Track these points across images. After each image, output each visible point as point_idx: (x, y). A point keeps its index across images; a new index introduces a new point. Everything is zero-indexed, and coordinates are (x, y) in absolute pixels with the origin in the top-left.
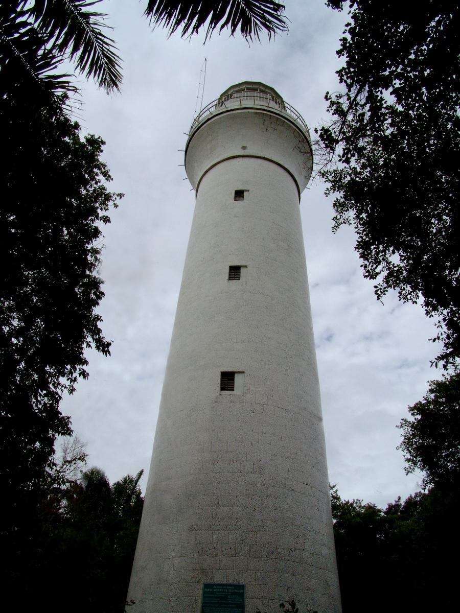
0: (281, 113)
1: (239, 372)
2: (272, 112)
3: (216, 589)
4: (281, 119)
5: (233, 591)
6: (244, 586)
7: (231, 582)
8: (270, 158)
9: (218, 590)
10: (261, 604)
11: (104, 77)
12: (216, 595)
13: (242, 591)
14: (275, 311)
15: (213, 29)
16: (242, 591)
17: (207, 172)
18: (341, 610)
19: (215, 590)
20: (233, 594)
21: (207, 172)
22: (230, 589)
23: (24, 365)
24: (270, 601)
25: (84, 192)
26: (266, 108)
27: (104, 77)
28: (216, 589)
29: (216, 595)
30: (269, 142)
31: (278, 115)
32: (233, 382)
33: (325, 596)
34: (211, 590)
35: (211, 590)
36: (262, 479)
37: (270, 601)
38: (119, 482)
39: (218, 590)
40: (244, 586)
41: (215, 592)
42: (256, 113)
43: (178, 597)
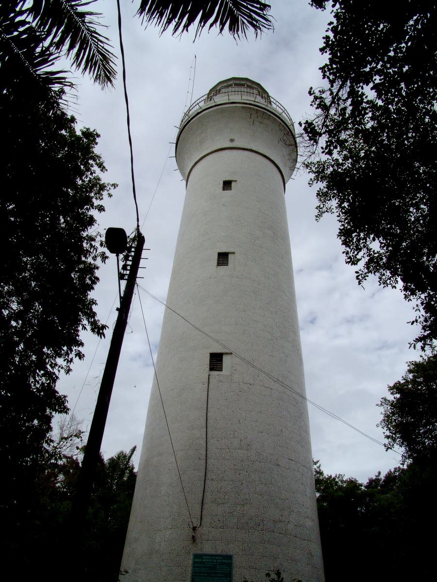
1: (227, 354)
2: (259, 107)
4: (267, 113)
6: (231, 556)
7: (219, 552)
8: (257, 150)
16: (230, 561)
17: (196, 163)
19: (204, 560)
20: (222, 563)
21: (196, 163)
24: (257, 571)
26: (252, 103)
29: (205, 565)
31: (264, 109)
32: (221, 362)
34: (201, 560)
35: (201, 560)
37: (257, 571)
39: (207, 560)
40: (231, 556)
42: (243, 107)
43: (169, 566)
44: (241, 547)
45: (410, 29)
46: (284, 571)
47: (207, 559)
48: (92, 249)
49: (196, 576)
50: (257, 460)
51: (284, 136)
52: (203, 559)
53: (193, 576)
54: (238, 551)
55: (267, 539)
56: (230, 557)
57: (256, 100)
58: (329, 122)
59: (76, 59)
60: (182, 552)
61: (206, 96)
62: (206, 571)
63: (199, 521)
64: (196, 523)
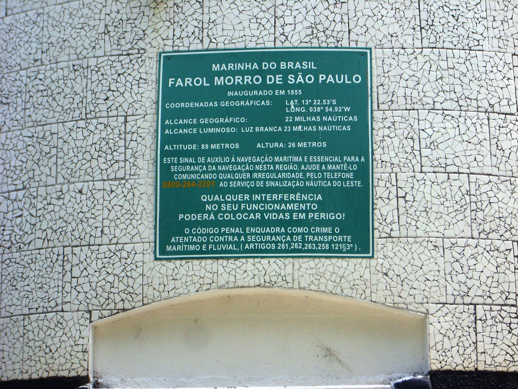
3: (224, 74)
5: (310, 79)
6: (364, 54)
9: (238, 79)
10: (452, 133)
12: (225, 104)
15: (394, 307)
16: (357, 79)
18: (4, 379)
19: (218, 81)
22: (295, 72)
24: (496, 120)
25: (300, 91)
28: (224, 74)
29: (225, 104)
34: (202, 82)
35: (202, 82)
37: (496, 120)
39: (238, 79)
40: (364, 54)
41: (225, 88)
43: (37, 123)
44: (409, 14)
46: (150, 229)
47: (233, 73)
48: (288, 205)
50: (324, 32)
52: (211, 76)
53: (164, 154)
54: (395, 28)
58: (295, 106)
60: (99, 52)
62: (233, 130)
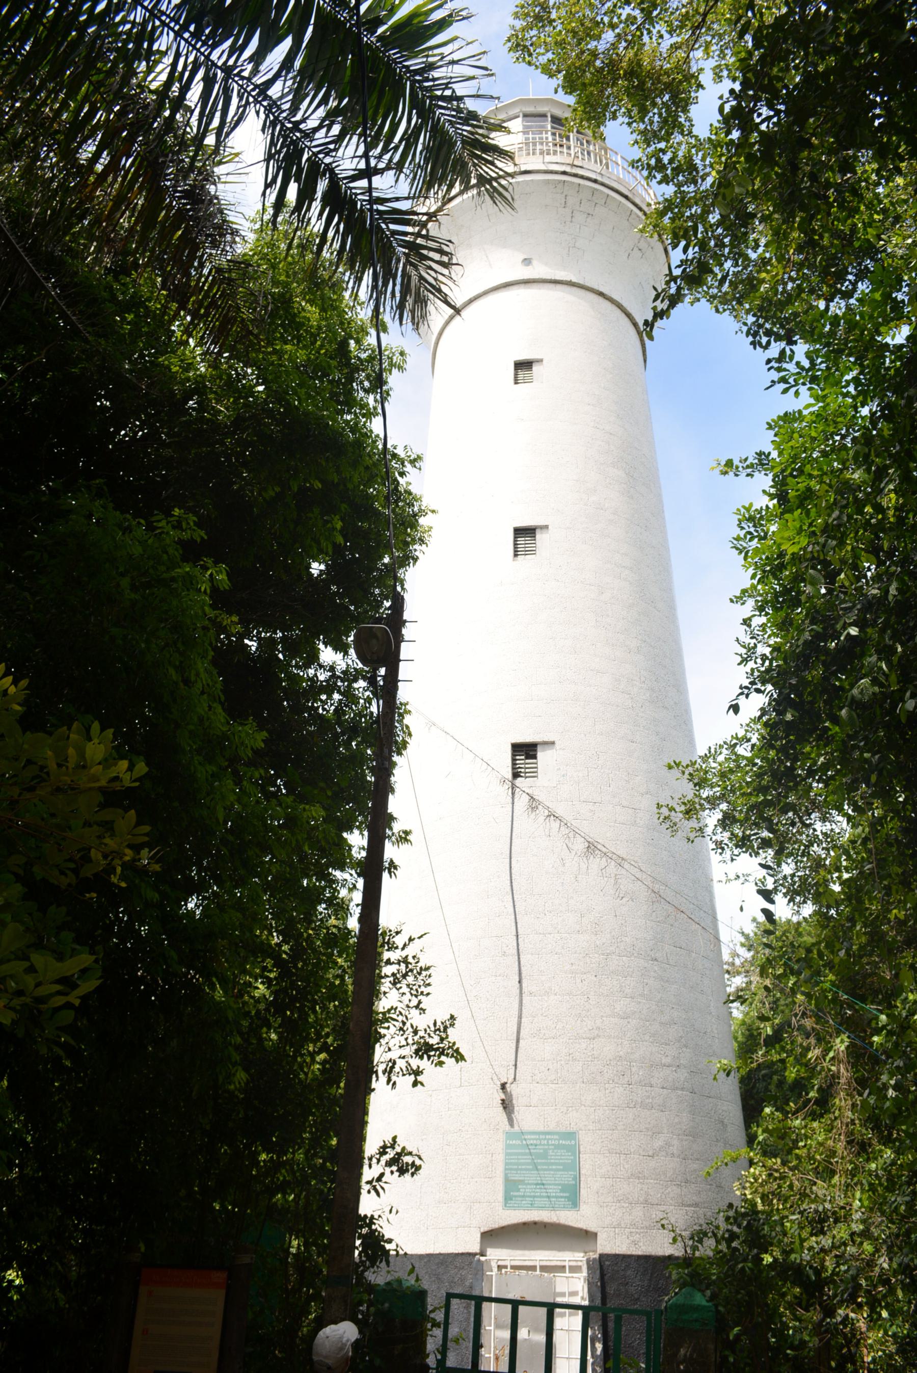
0: (599, 178)
1: (545, 743)
2: (582, 177)
4: (602, 192)
5: (557, 1142)
7: (552, 1127)
8: (581, 282)
11: (241, 110)
13: (573, 1142)
14: (608, 616)
16: (573, 1142)
17: (601, 294)
20: (558, 1147)
21: (601, 294)
22: (551, 1139)
23: (235, 619)
24: (623, 1157)
26: (568, 169)
27: (241, 110)
30: (577, 245)
31: (595, 181)
32: (534, 761)
33: (719, 1144)
36: (598, 942)
38: (542, 73)
42: (548, 182)
43: (460, 1155)
45: (724, 246)
49: (511, 1169)
51: (640, 239)
53: (506, 1169)
55: (640, 1100)
56: (571, 1135)
57: (576, 163)
59: (353, 176)
61: (169, 68)
63: (512, 1071)
64: (506, 1077)
